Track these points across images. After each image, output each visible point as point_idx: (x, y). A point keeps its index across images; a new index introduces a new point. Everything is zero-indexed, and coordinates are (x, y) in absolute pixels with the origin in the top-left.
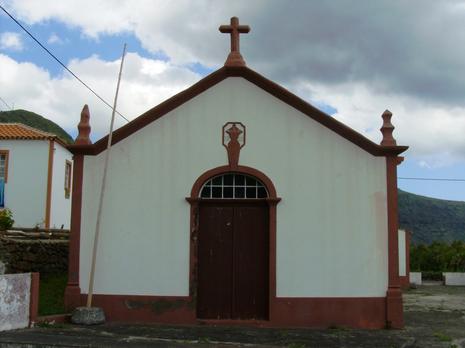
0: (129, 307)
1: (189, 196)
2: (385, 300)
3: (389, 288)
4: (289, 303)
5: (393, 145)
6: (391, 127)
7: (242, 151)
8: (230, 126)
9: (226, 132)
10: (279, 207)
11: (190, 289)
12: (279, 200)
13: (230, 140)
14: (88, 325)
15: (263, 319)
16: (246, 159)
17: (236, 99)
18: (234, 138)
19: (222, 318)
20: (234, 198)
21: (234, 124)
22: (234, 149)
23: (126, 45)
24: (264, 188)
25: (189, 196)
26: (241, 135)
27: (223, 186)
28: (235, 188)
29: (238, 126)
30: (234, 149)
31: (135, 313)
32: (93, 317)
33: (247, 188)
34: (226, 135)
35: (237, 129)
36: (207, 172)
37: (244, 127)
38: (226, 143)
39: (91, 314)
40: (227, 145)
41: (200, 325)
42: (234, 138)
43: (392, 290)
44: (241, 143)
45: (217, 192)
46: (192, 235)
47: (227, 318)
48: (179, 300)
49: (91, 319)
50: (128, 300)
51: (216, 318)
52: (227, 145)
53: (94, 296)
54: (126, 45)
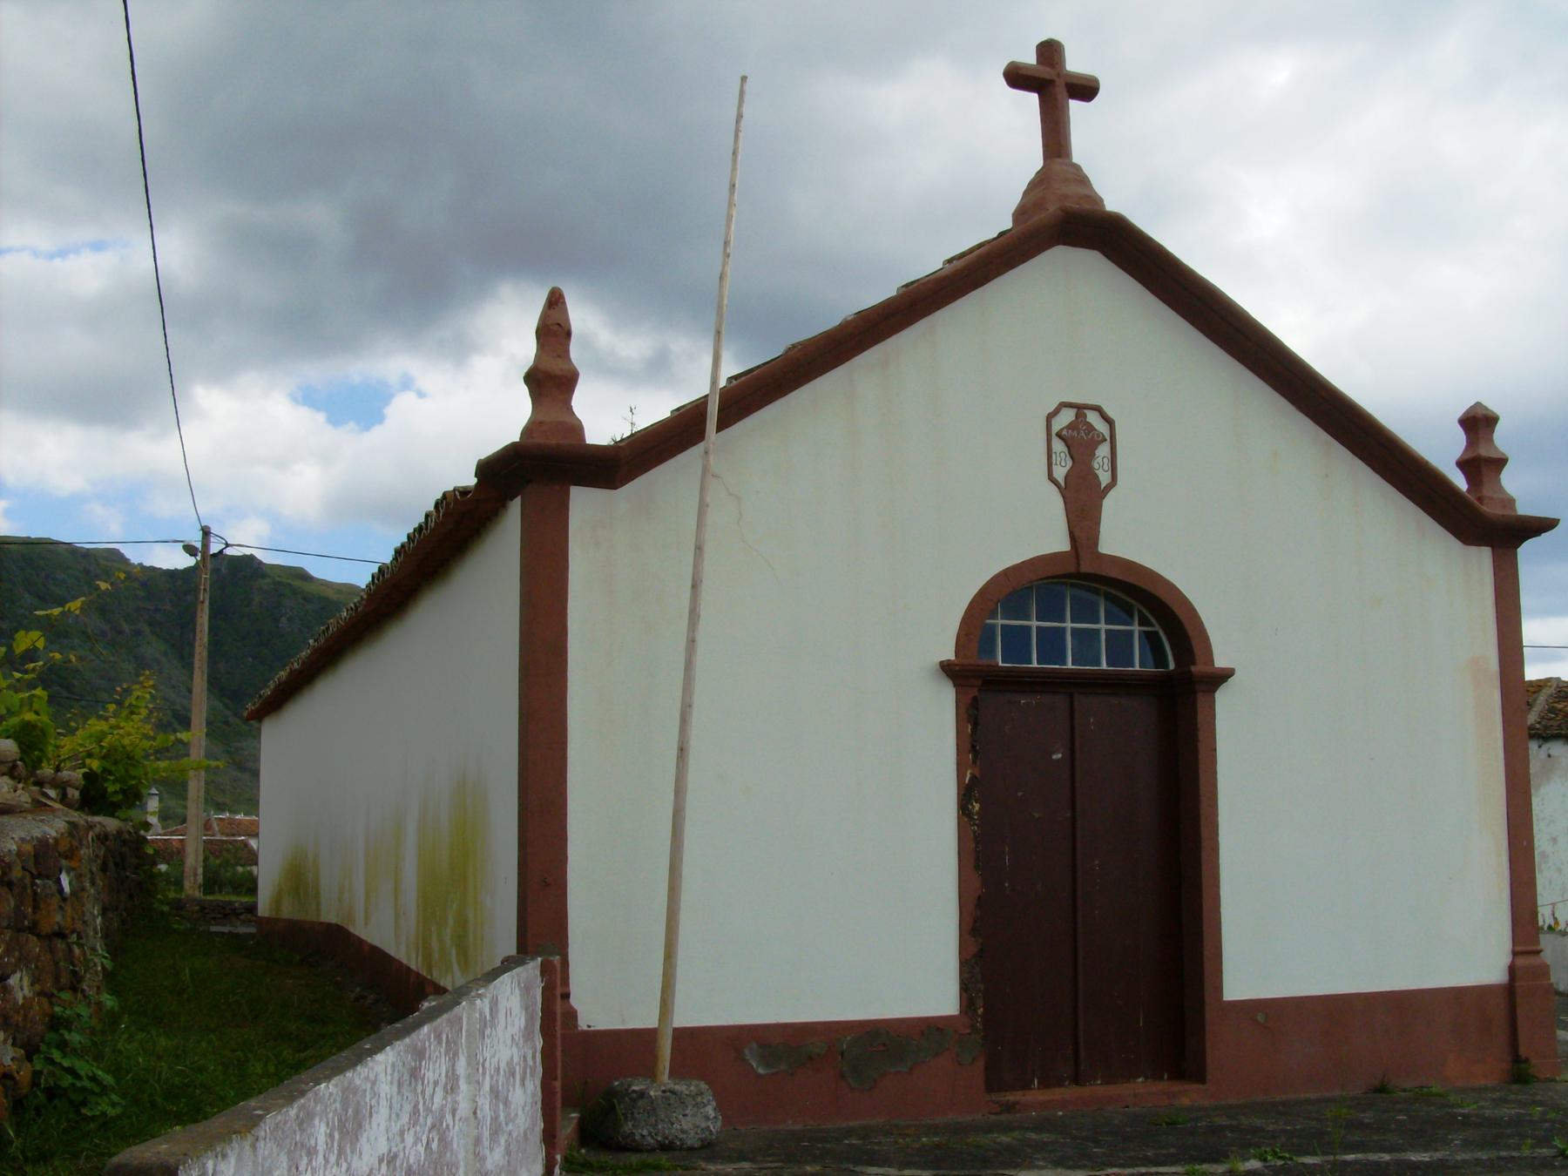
0: (761, 1071)
1: (950, 655)
2: (1510, 991)
3: (1515, 953)
4: (1260, 1018)
5: (1507, 512)
6: (1494, 455)
7: (1109, 503)
8: (1067, 417)
9: (1059, 435)
10: (1224, 699)
11: (965, 987)
12: (1225, 676)
13: (1070, 463)
14: (691, 1149)
15: (1170, 1079)
16: (1124, 536)
17: (1071, 319)
18: (1082, 456)
19: (1046, 1084)
20: (1070, 665)
21: (1080, 409)
22: (1083, 497)
23: (744, 79)
24: (1156, 633)
25: (950, 655)
26: (1103, 451)
27: (1103, 626)
28: (1098, 631)
29: (1093, 418)
30: (1083, 497)
31: (808, 1087)
32: (707, 1118)
33: (1107, 631)
34: (1058, 446)
35: (1091, 428)
36: (1006, 572)
37: (1110, 422)
38: (1060, 473)
39: (696, 1105)
40: (1061, 481)
41: (1001, 1113)
42: (1082, 456)
43: (1521, 961)
44: (1104, 478)
45: (1016, 641)
46: (966, 795)
47: (1060, 1084)
48: (929, 1029)
49: (703, 1125)
50: (755, 1045)
51: (1026, 1086)
52: (1061, 481)
53: (685, 1036)
54: (744, 79)
